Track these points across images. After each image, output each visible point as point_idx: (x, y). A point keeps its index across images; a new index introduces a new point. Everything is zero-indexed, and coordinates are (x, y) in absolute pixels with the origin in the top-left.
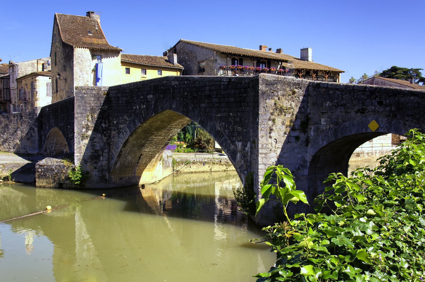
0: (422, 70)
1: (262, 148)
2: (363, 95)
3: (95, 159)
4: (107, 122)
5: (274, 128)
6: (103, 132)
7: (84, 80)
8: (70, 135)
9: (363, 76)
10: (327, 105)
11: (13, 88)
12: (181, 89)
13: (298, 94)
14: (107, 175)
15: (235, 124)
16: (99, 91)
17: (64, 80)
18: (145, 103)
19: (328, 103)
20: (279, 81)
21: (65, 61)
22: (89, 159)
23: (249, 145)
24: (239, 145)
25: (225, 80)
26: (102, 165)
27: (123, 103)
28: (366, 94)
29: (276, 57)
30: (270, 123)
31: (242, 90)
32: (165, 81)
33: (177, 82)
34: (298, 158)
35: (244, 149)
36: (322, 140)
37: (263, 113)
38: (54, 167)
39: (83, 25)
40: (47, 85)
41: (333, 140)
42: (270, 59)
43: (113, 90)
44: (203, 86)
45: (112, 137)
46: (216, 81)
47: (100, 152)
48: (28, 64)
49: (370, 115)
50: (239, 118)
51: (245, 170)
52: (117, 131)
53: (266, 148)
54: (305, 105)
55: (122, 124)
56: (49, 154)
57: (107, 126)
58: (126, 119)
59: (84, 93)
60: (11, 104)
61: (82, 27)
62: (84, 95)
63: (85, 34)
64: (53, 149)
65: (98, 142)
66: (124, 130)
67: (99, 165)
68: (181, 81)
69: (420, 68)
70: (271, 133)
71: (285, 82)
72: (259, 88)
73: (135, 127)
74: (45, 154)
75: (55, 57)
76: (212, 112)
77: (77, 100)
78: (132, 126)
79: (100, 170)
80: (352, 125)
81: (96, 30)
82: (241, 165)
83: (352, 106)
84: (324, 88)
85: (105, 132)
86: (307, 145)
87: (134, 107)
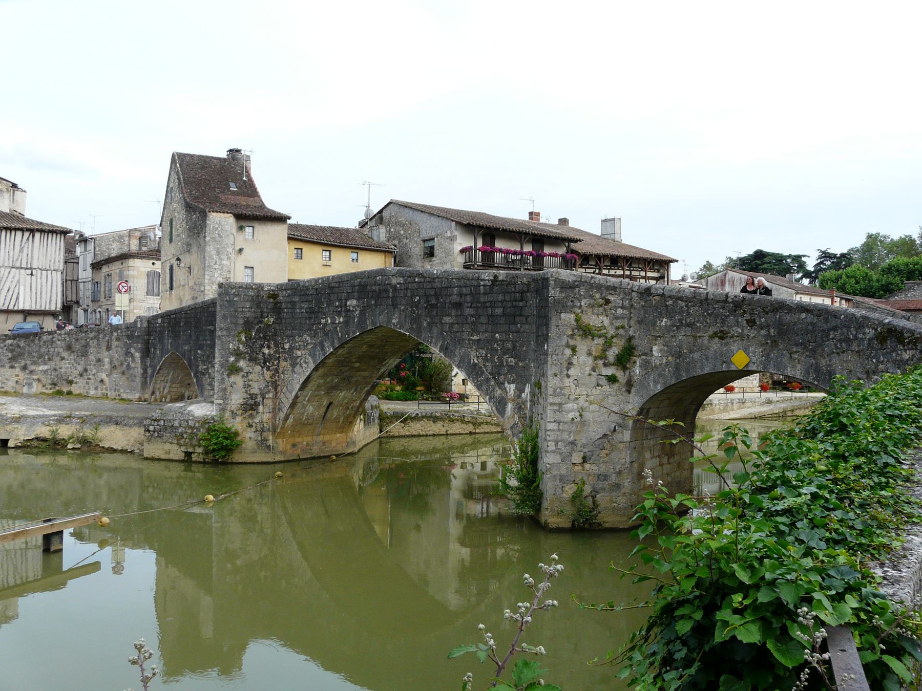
0: (808, 257)
2: (723, 308)
3: (249, 410)
5: (575, 362)
6: (265, 363)
7: (222, 269)
8: (201, 366)
9: (705, 266)
10: (663, 323)
11: (84, 280)
12: (409, 291)
13: (614, 305)
14: (271, 438)
15: (505, 354)
16: (259, 292)
17: (187, 269)
18: (344, 314)
19: (665, 320)
21: (189, 236)
23: (528, 389)
24: (511, 388)
25: (487, 278)
26: (262, 420)
27: (303, 312)
28: (727, 306)
29: (559, 233)
30: (568, 352)
31: (517, 294)
32: (380, 277)
33: (401, 279)
35: (519, 396)
36: (654, 381)
37: (556, 336)
38: (176, 424)
40: (147, 275)
41: (673, 382)
42: (497, 229)
43: (285, 290)
44: (448, 287)
45: (280, 371)
46: (471, 278)
47: (259, 399)
48: (113, 237)
49: (734, 341)
50: (510, 343)
51: (521, 433)
52: (289, 362)
53: (561, 394)
55: (299, 349)
56: (159, 400)
57: (272, 352)
58: (307, 341)
59: (234, 294)
60: (78, 307)
61: (219, 175)
64: (166, 391)
66: (303, 359)
68: (408, 277)
69: (804, 254)
73: (324, 355)
74: (152, 400)
75: (169, 228)
76: (463, 332)
77: (221, 306)
78: (317, 353)
79: (259, 429)
80: (704, 357)
82: (515, 424)
83: (705, 327)
84: (659, 295)
86: (629, 392)
87: (323, 321)
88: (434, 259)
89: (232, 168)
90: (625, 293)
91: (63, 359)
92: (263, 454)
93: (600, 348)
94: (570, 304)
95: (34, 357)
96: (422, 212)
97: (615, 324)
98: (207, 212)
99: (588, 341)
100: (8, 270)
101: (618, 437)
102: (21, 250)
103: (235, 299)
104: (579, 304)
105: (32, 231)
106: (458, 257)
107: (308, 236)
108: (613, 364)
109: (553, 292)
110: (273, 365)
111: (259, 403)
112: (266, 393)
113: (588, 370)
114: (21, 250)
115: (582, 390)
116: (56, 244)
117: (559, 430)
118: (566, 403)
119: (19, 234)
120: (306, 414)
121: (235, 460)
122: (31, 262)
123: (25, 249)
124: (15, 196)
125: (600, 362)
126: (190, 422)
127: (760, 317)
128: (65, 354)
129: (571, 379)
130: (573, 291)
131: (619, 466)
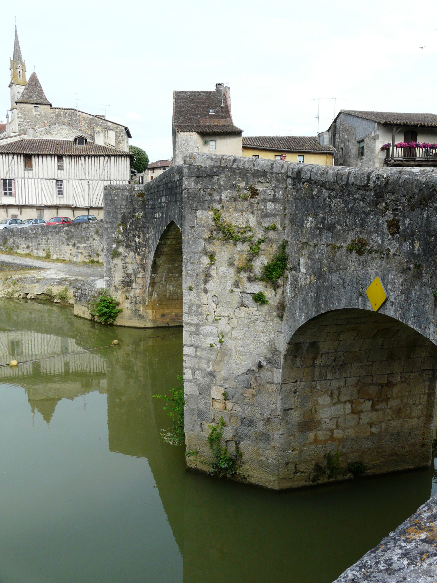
1: (190, 313)
3: (127, 286)
4: (141, 236)
5: (213, 273)
6: (136, 250)
13: (262, 197)
14: (141, 308)
20: (222, 167)
22: (120, 285)
30: (206, 260)
34: (262, 342)
37: (190, 239)
39: (206, 102)
42: (415, 126)
47: (133, 278)
49: (373, 259)
54: (279, 222)
57: (141, 241)
59: (114, 194)
61: (203, 104)
62: (114, 197)
63: (205, 114)
65: (130, 263)
67: (132, 295)
70: (208, 284)
71: (235, 168)
72: (184, 186)
81: (222, 107)
85: (139, 250)
88: (363, 157)
89: (215, 98)
90: (278, 180)
91: (94, 239)
92: (137, 321)
93: (245, 256)
94: (207, 197)
95: (78, 238)
96: (358, 117)
97: (264, 225)
98: (176, 132)
99: (230, 247)
100: (97, 182)
101: (266, 374)
102: (104, 169)
103: (116, 198)
104: (218, 198)
105: (109, 156)
106: (379, 154)
107: (263, 146)
108: (261, 280)
109: (186, 183)
110: (142, 251)
111: (133, 281)
112: (138, 273)
113: (229, 284)
114: (104, 169)
115: (224, 311)
116: (124, 163)
117: (196, 357)
118: (205, 325)
119: (102, 158)
120: (168, 291)
121: (118, 324)
122: (110, 176)
123: (106, 168)
124: (108, 135)
125: (244, 275)
126: (93, 292)
127: (404, 216)
128: (95, 237)
129: (210, 295)
130: (211, 181)
131: (268, 413)
